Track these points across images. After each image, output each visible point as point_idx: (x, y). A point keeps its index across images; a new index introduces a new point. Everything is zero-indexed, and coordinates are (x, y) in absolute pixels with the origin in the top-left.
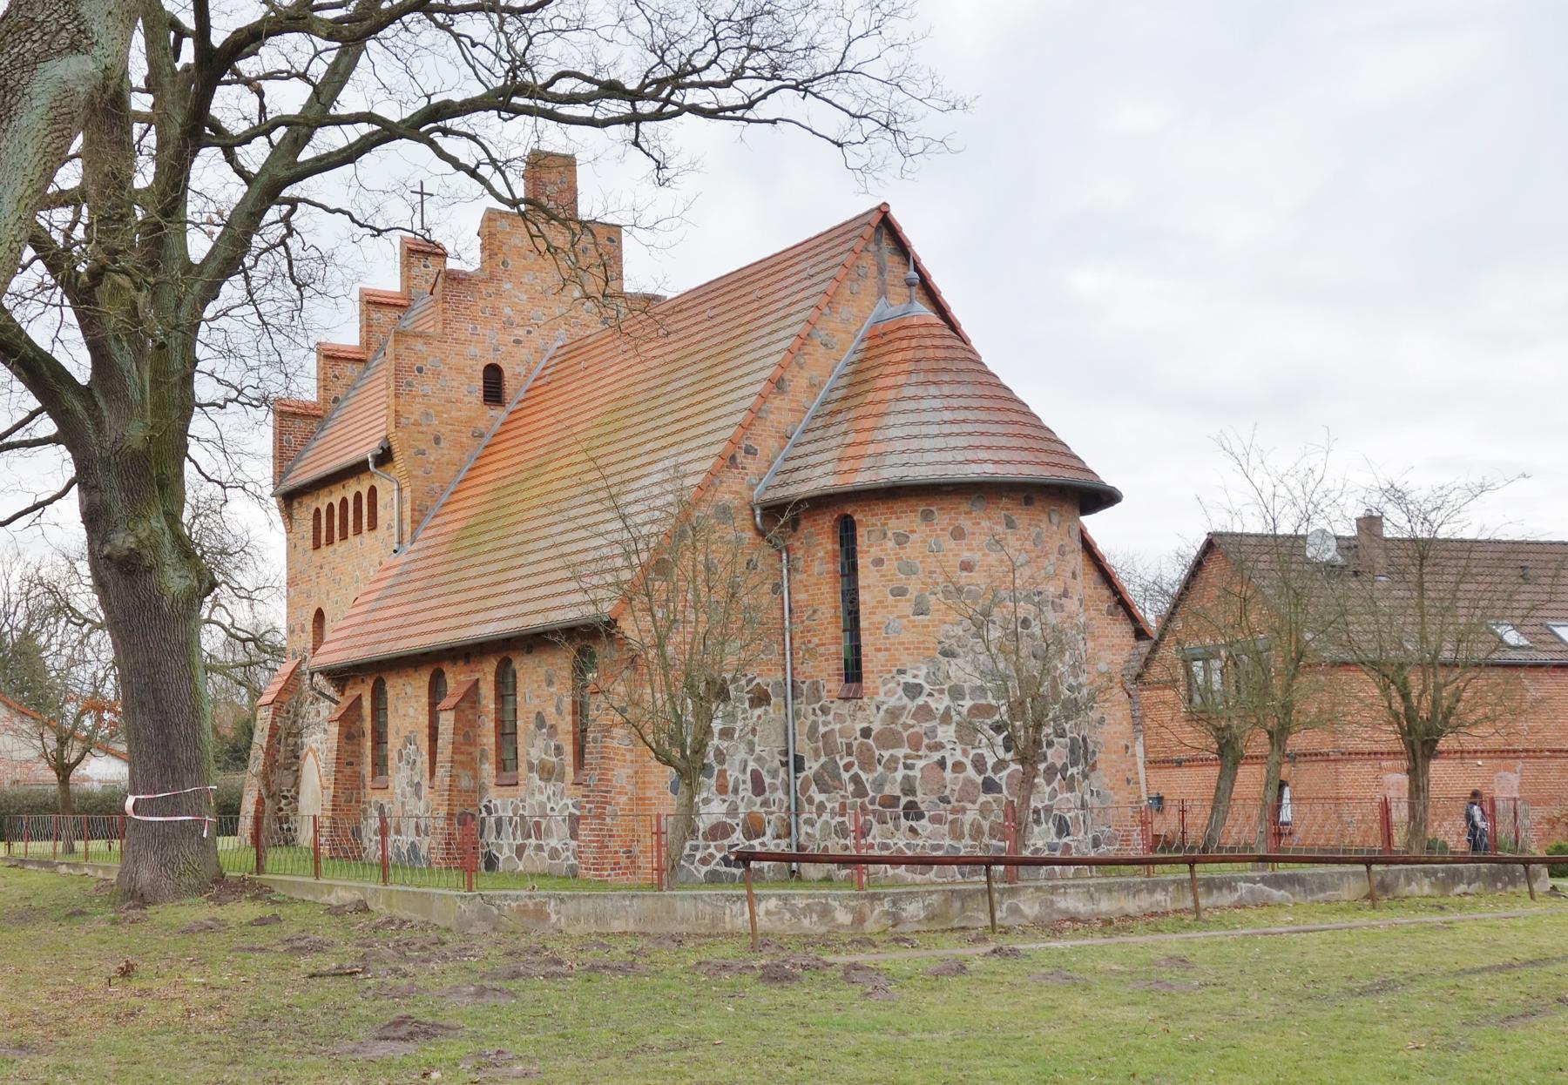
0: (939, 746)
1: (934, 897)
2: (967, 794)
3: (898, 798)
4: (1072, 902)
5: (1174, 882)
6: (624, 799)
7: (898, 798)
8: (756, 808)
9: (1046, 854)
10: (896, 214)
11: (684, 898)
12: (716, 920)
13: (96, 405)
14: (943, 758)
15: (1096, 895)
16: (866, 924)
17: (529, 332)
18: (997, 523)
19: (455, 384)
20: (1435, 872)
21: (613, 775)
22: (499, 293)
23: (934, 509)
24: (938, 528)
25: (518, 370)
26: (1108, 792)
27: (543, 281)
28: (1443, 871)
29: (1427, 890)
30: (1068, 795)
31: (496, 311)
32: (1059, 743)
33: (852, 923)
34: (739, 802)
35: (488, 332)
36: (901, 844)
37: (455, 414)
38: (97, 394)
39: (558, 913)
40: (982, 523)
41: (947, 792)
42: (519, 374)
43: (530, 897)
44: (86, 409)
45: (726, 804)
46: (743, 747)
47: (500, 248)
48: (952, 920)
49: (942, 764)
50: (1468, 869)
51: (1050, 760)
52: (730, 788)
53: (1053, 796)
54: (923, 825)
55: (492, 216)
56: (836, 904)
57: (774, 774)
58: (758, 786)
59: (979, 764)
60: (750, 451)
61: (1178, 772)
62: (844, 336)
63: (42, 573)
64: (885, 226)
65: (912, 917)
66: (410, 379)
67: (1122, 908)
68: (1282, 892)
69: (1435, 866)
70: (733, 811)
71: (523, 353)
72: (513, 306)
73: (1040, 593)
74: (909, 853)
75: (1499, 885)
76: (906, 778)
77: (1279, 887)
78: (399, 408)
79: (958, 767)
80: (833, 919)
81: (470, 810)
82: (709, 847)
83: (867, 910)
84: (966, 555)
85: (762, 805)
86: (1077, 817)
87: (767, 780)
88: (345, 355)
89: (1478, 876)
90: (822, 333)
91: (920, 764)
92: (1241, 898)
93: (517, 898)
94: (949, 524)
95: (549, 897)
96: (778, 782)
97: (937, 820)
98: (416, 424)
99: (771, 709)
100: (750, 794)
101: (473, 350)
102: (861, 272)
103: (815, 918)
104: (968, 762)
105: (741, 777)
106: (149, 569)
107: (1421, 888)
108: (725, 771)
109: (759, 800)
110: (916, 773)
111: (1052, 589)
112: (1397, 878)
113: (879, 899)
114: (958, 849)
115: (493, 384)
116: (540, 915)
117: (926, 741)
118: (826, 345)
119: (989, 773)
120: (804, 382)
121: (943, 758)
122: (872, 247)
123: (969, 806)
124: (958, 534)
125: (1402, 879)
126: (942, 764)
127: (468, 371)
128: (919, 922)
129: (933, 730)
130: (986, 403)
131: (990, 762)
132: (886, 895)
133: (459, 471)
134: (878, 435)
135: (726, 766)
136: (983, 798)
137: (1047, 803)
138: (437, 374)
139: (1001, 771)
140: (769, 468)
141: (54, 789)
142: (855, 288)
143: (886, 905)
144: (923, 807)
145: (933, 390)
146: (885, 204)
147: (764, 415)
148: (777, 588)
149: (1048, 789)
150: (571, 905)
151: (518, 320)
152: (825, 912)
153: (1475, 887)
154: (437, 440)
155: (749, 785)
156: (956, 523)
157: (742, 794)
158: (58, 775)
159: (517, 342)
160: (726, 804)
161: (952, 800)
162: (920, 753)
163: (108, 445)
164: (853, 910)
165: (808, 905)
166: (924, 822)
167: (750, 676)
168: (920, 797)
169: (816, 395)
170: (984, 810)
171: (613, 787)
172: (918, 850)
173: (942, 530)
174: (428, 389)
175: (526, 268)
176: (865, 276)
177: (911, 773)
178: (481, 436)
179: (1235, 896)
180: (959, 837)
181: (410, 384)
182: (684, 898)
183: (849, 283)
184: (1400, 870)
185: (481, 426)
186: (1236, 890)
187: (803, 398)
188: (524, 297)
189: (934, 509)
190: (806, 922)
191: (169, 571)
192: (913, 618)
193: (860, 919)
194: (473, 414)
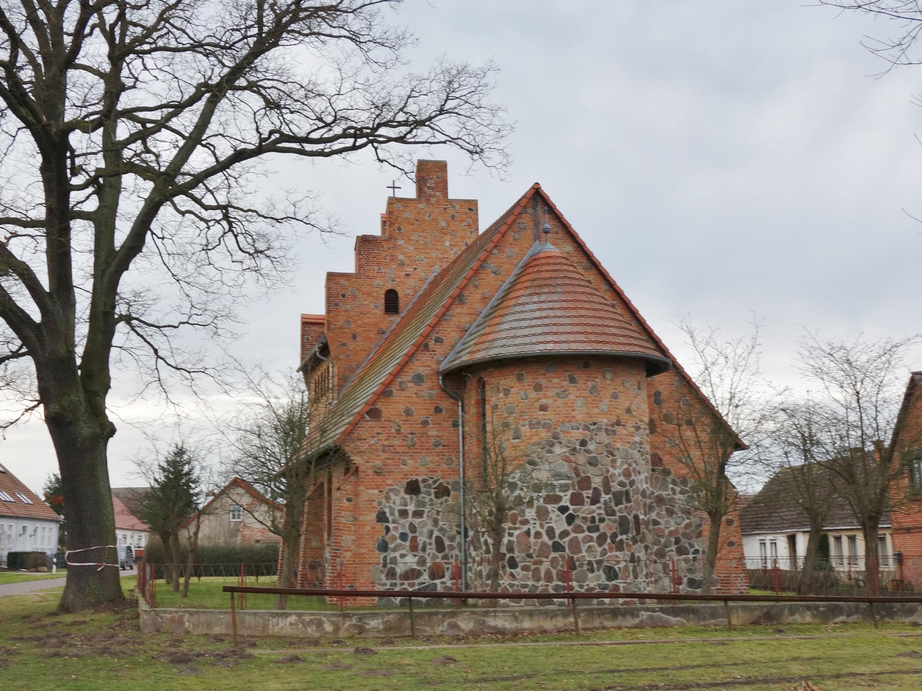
0: (526, 522)
1: (391, 616)
2: (543, 551)
3: (505, 555)
4: (501, 622)
5: (586, 610)
6: (349, 554)
7: (505, 555)
8: (438, 560)
9: (597, 590)
10: (546, 189)
11: (250, 614)
12: (265, 627)
13: (42, 333)
14: (529, 529)
15: (520, 618)
16: (340, 632)
17: (415, 269)
18: (563, 381)
19: (366, 303)
20: (817, 608)
21: (342, 540)
22: (395, 247)
23: (523, 373)
24: (526, 384)
25: (408, 292)
27: (425, 237)
28: (824, 606)
29: (808, 619)
30: (618, 553)
31: (393, 258)
32: (609, 520)
33: (333, 631)
34: (426, 556)
35: (388, 271)
36: (506, 583)
37: (366, 320)
38: (43, 328)
39: (189, 621)
40: (555, 382)
41: (531, 551)
42: (409, 295)
43: (177, 612)
44: (36, 336)
45: (417, 558)
46: (430, 523)
47: (396, 220)
48: (405, 631)
49: (528, 533)
50: (849, 606)
51: (602, 530)
52: (420, 548)
53: (604, 553)
54: (518, 571)
55: (391, 202)
56: (325, 619)
57: (452, 539)
58: (440, 546)
59: (551, 532)
60: (439, 341)
61: (908, 536)
62: (509, 266)
64: (537, 196)
65: (374, 628)
66: (337, 301)
67: (541, 626)
68: (678, 618)
69: (817, 603)
70: (422, 562)
71: (411, 282)
72: (405, 254)
73: (595, 424)
74: (511, 590)
76: (509, 541)
77: (676, 615)
78: (330, 319)
79: (538, 535)
80: (324, 629)
81: (318, 560)
82: (403, 584)
83: (341, 624)
84: (543, 401)
85: (443, 558)
86: (626, 567)
87: (447, 543)
89: (857, 611)
90: (492, 265)
91: (516, 533)
92: (642, 621)
93: (171, 612)
94: (533, 382)
95: (185, 612)
96: (455, 544)
97: (525, 568)
98: (341, 328)
99: (450, 499)
100: (434, 551)
101: (378, 282)
102: (522, 226)
103: (314, 628)
104: (543, 532)
105: (428, 541)
106: (70, 423)
107: (803, 617)
108: (416, 537)
109: (440, 555)
110: (514, 539)
111: (606, 421)
112: (782, 611)
113: (349, 617)
114: (537, 587)
115: (392, 302)
116: (181, 622)
117: (519, 518)
118: (495, 273)
119: (557, 539)
120: (478, 297)
121: (529, 529)
122: (530, 210)
123: (544, 559)
124: (538, 388)
125: (786, 611)
126: (528, 533)
127: (375, 294)
128: (379, 632)
129: (523, 512)
130: (565, 305)
131: (557, 532)
132: (354, 615)
133: (369, 355)
134: (497, 328)
135: (416, 534)
136: (553, 555)
137: (599, 558)
138: (354, 297)
139: (564, 537)
140: (452, 349)
142: (517, 236)
143: (354, 621)
144: (517, 560)
145: (535, 299)
146: (537, 183)
147: (449, 318)
148: (455, 425)
149: (599, 549)
150: (196, 617)
151: (407, 262)
152: (320, 624)
153: (854, 618)
154: (354, 337)
155: (434, 546)
156: (537, 381)
157: (428, 551)
158: (162, 538)
159: (407, 275)
160: (417, 558)
161: (534, 556)
162: (516, 526)
163: (47, 355)
164: (333, 623)
165: (311, 620)
166: (519, 570)
167: (435, 478)
168: (516, 554)
169: (487, 304)
170: (554, 561)
171: (342, 547)
172: (515, 588)
173: (529, 386)
174: (348, 307)
175: (414, 231)
176: (525, 229)
177: (511, 539)
178: (383, 333)
179: (637, 620)
180: (538, 580)
181: (337, 305)
182: (250, 614)
183: (513, 234)
184: (784, 605)
185: (383, 327)
186: (638, 616)
187: (478, 307)
188: (412, 248)
189: (523, 373)
190: (309, 630)
191: (82, 424)
192: (512, 441)
193: (337, 630)
194: (378, 320)
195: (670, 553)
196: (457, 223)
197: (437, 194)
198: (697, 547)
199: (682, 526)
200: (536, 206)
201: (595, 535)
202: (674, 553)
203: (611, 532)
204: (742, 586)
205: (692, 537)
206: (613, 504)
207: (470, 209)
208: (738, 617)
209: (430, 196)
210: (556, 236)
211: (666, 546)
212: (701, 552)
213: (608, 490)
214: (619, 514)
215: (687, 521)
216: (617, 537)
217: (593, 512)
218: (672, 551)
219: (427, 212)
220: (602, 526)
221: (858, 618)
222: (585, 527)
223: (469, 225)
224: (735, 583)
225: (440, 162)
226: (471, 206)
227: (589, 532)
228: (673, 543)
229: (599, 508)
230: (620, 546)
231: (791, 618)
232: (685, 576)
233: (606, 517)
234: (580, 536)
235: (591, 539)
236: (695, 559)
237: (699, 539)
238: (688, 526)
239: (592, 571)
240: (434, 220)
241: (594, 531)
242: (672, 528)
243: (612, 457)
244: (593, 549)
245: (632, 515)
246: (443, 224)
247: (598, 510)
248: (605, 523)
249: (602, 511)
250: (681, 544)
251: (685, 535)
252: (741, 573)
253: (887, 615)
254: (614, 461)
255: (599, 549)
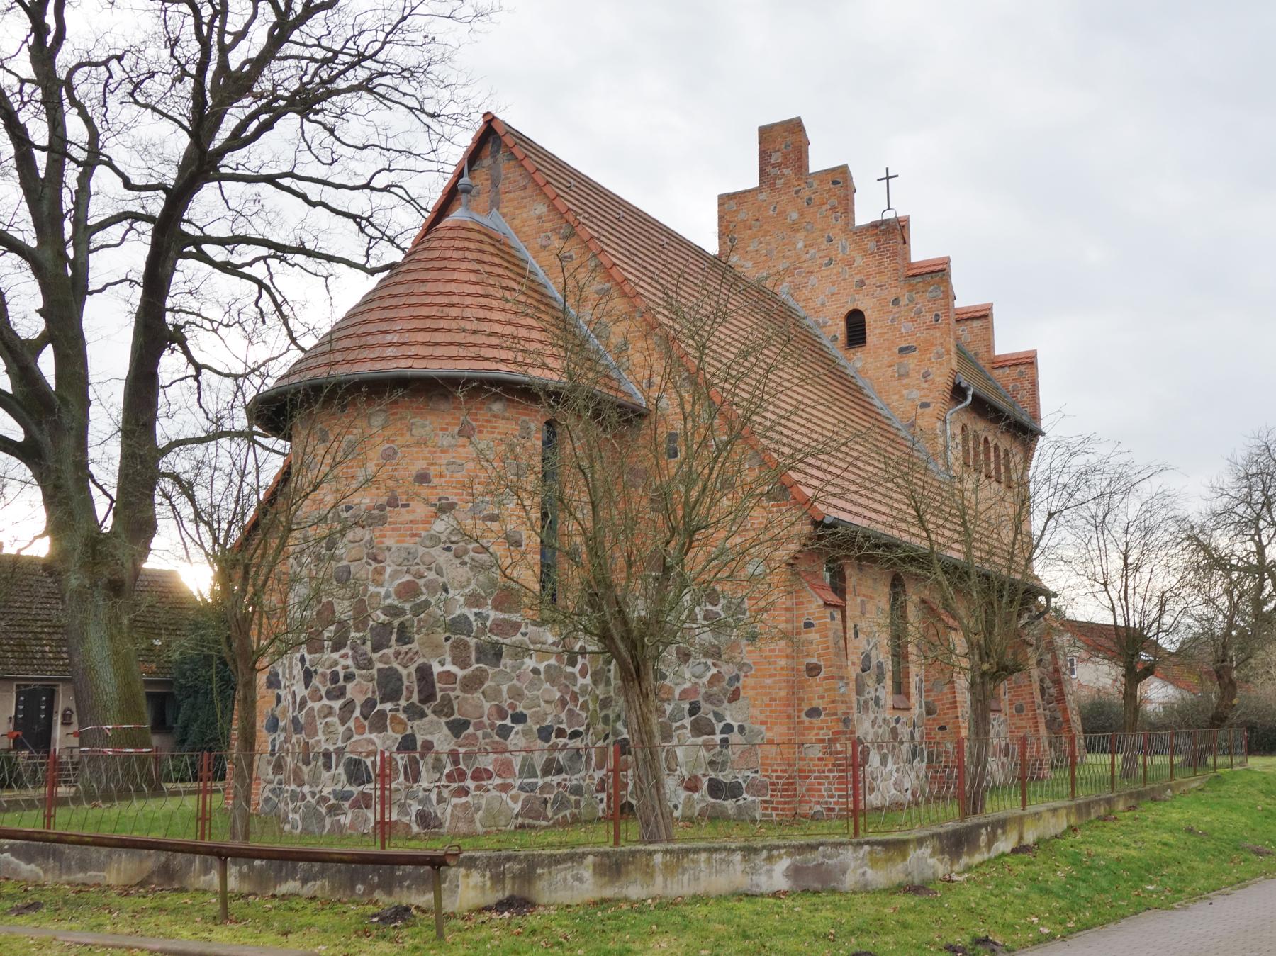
10: (515, 117)
26: (757, 727)
27: (768, 243)
30: (373, 736)
51: (349, 696)
63: (1203, 512)
68: (32, 866)
75: (360, 888)
88: (969, 315)
137: (340, 744)
141: (1117, 698)
149: (341, 729)
188: (749, 264)
195: (678, 732)
196: (816, 209)
197: (786, 171)
198: (729, 720)
199: (705, 680)
200: (498, 151)
201: (337, 704)
202: (687, 732)
203: (363, 699)
204: (831, 796)
205: (721, 702)
206: (368, 647)
207: (835, 183)
208: (118, 870)
209: (776, 177)
210: (522, 193)
211: (674, 718)
212: (736, 729)
213: (361, 621)
214: (379, 665)
215: (714, 671)
216: (375, 706)
217: (336, 663)
218: (683, 727)
219: (770, 203)
220: (349, 687)
221: (323, 887)
222: (323, 691)
223: (833, 208)
224: (820, 790)
225: (790, 121)
226: (840, 179)
227: (328, 699)
228: (686, 713)
229: (345, 656)
230: (379, 724)
231: (202, 878)
232: (704, 775)
233: (357, 672)
234: (317, 705)
235: (330, 711)
236: (724, 742)
237: (734, 704)
238: (715, 679)
239: (328, 767)
240: (781, 213)
241: (338, 698)
242: (687, 685)
243: (374, 565)
244: (332, 729)
245: (413, 668)
246: (795, 216)
247: (343, 661)
248: (355, 682)
249: (350, 662)
250: (701, 714)
251: (709, 698)
252: (830, 771)
253: (379, 886)
254: (379, 572)
255: (341, 729)
